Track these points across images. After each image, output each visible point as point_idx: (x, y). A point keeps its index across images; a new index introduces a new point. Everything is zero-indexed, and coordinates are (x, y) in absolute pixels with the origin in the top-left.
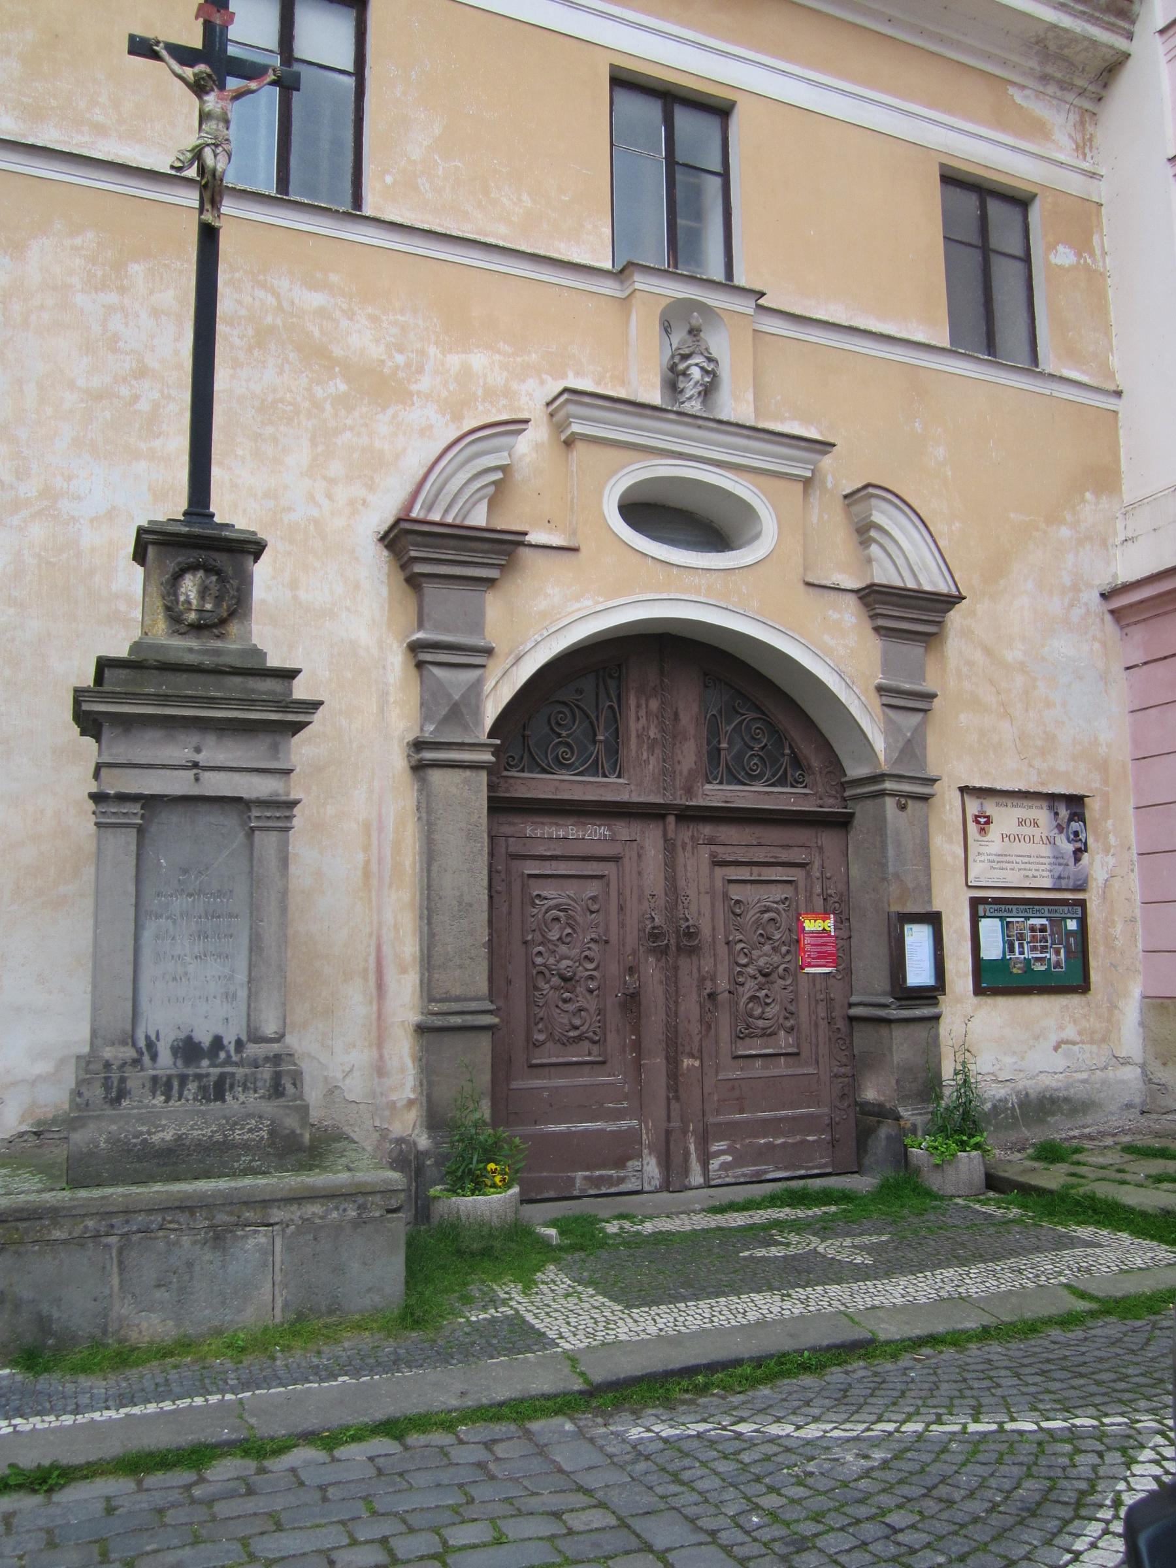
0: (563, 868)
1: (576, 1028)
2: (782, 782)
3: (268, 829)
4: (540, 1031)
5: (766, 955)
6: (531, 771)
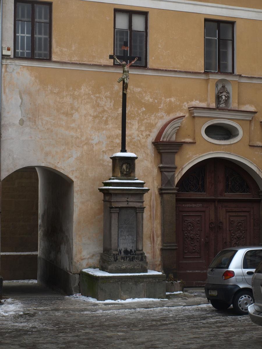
1: (194, 250)
2: (244, 192)
3: (140, 212)
4: (186, 250)
5: (239, 233)
6: (184, 192)
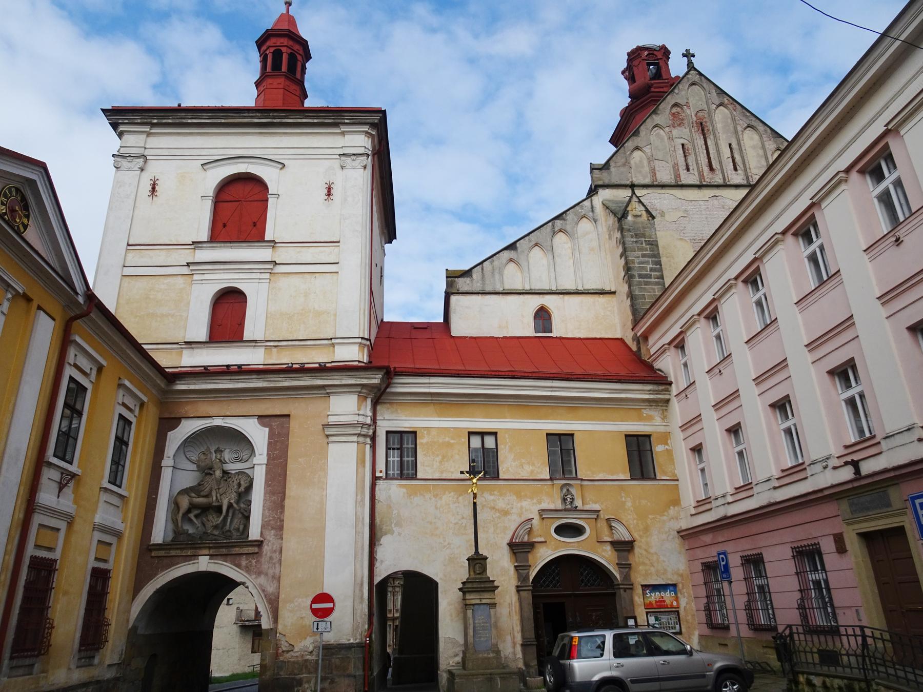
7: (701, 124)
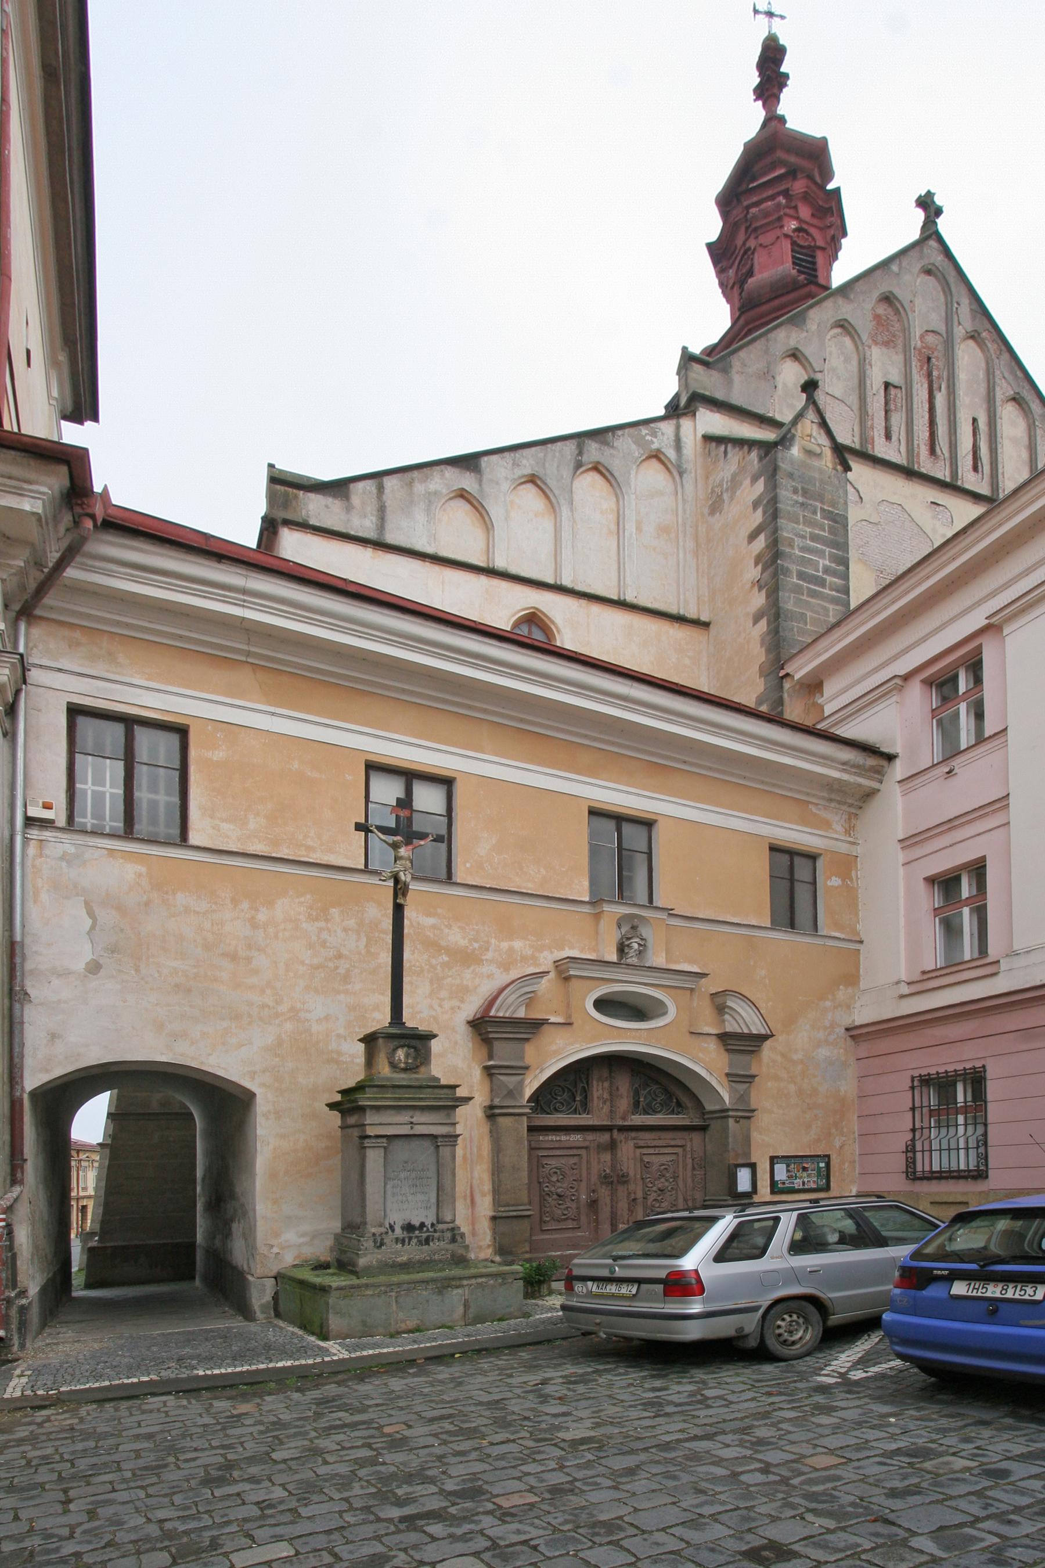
0: (558, 1152)
2: (672, 1113)
7: (929, 359)
